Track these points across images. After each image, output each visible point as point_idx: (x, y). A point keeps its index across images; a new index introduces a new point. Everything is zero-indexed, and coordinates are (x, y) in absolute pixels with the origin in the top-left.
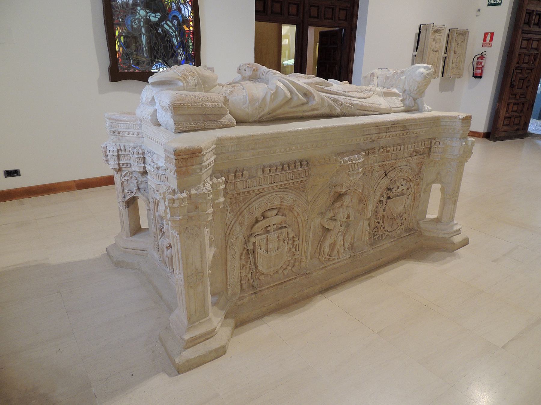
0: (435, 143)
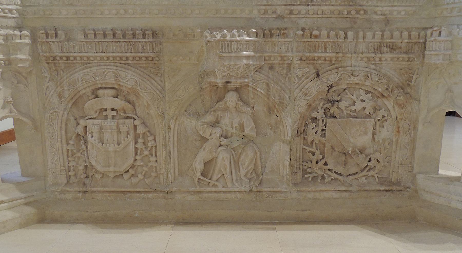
0: (432, 35)
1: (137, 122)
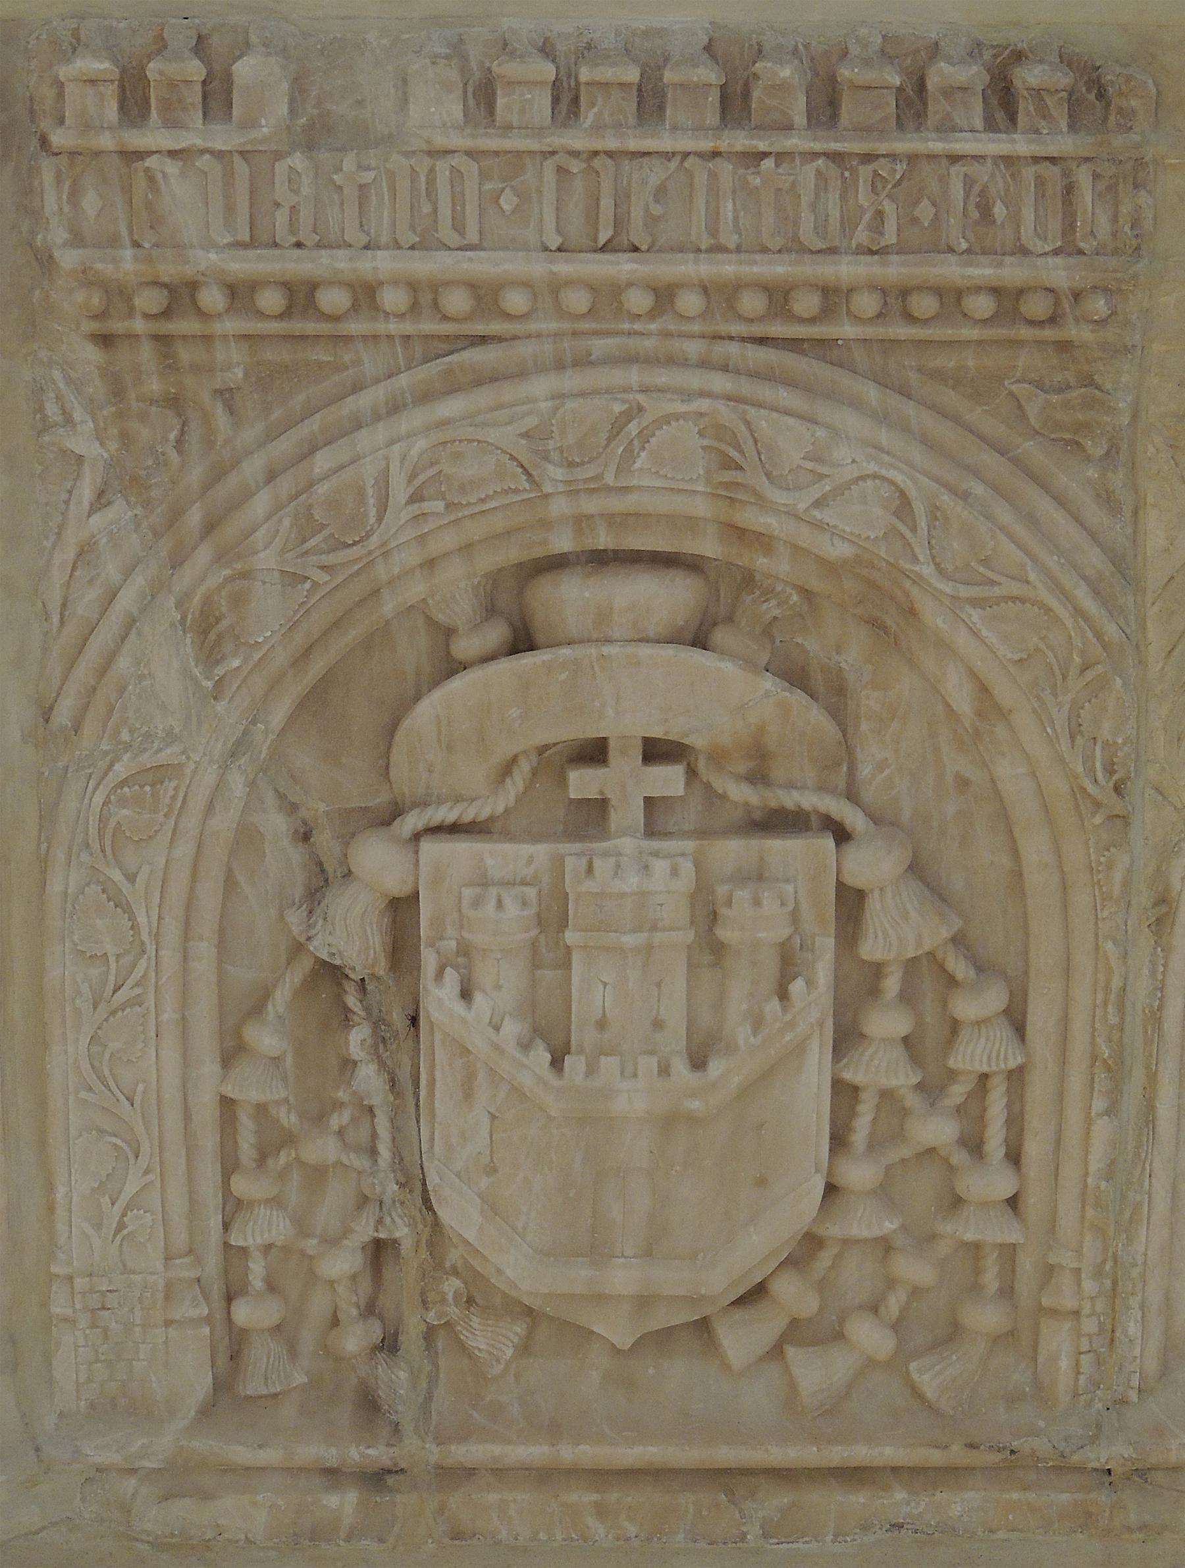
1: (873, 864)
